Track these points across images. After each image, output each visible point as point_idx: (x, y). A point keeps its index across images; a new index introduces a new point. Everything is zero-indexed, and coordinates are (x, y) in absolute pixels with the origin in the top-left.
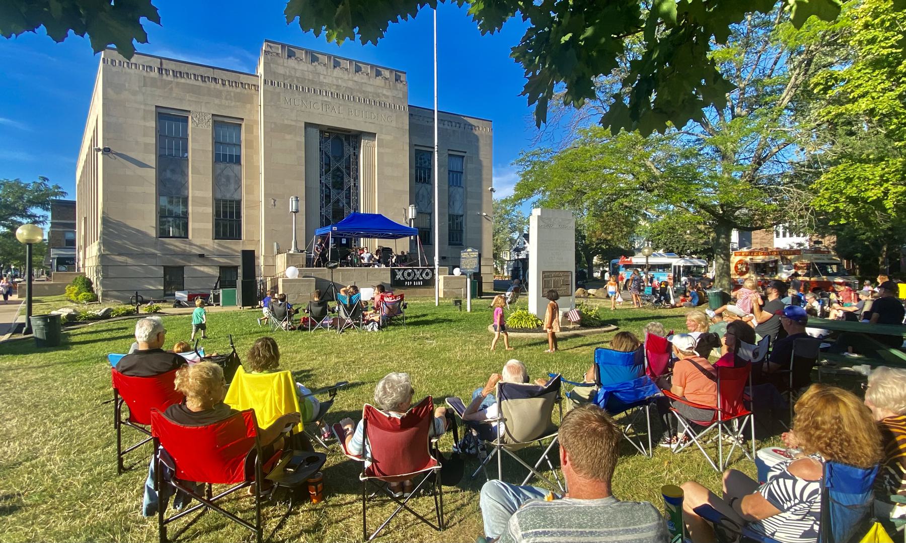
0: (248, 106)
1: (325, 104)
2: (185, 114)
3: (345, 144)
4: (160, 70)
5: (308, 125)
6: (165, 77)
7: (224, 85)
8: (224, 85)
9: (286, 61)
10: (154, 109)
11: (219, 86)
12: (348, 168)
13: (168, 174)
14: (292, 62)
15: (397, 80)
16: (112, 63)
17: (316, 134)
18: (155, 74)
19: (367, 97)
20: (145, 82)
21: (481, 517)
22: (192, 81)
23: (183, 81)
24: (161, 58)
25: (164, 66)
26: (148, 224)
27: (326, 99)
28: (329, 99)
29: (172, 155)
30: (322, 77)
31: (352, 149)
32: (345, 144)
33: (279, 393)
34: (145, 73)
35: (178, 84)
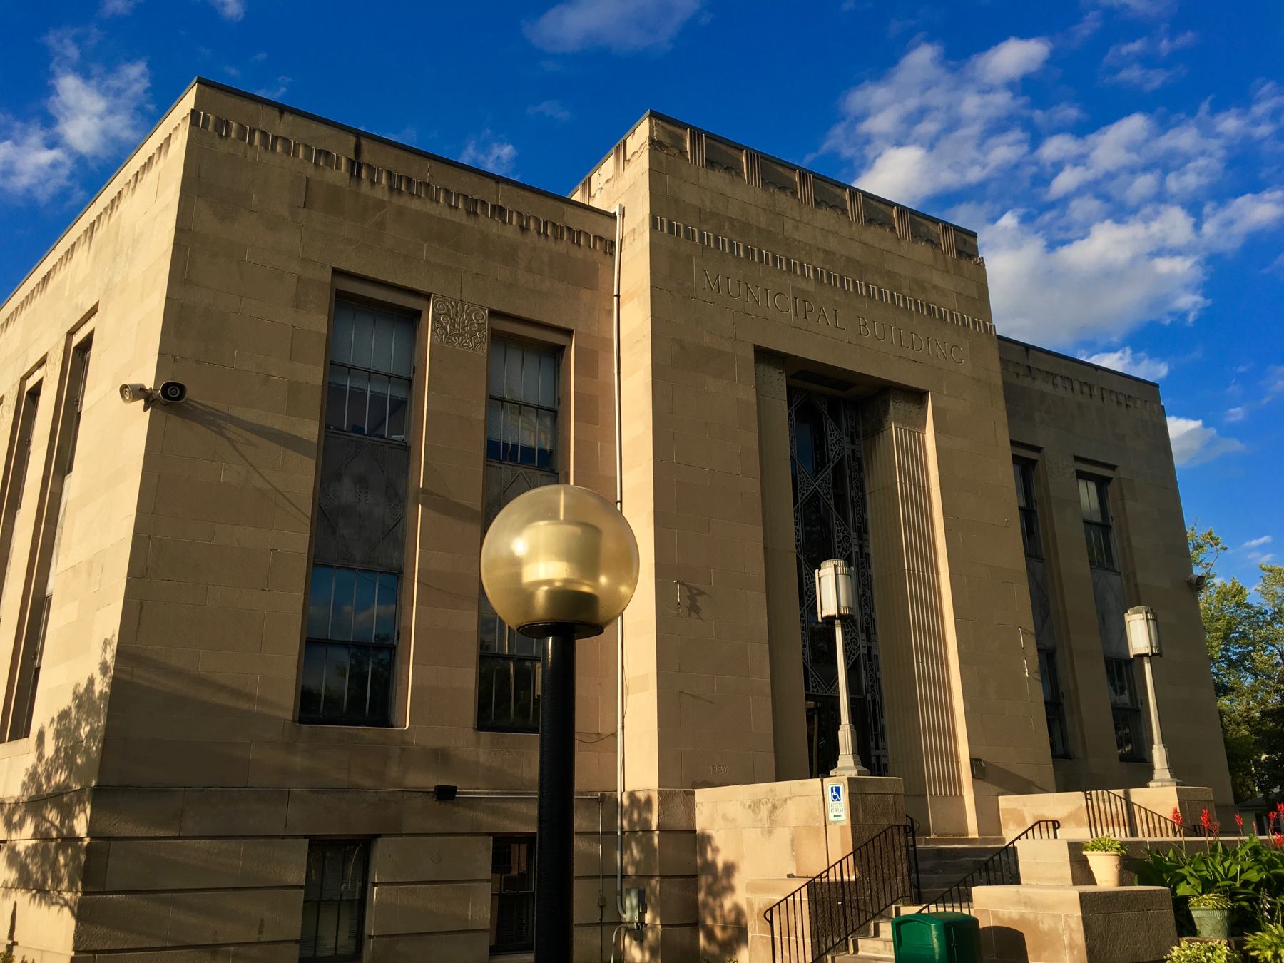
0: (586, 295)
1: (802, 298)
2: (412, 303)
3: (829, 424)
4: (355, 166)
5: (764, 356)
6: (365, 187)
7: (524, 229)
8: (524, 229)
9: (702, 172)
10: (327, 276)
11: (510, 231)
12: (840, 499)
13: (347, 492)
14: (718, 179)
15: (960, 253)
16: (218, 128)
17: (778, 381)
18: (339, 175)
19: (899, 290)
20: (308, 195)
21: (308, 621)
22: (439, 210)
23: (415, 204)
24: (358, 134)
25: (366, 157)
26: (274, 674)
27: (802, 285)
28: (811, 287)
29: (359, 430)
30: (789, 225)
31: (846, 440)
32: (829, 424)
33: (70, 252)
34: (310, 171)
35: (401, 212)
